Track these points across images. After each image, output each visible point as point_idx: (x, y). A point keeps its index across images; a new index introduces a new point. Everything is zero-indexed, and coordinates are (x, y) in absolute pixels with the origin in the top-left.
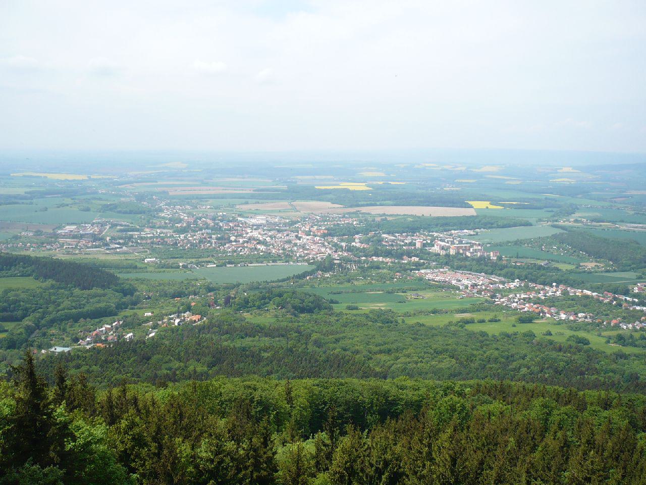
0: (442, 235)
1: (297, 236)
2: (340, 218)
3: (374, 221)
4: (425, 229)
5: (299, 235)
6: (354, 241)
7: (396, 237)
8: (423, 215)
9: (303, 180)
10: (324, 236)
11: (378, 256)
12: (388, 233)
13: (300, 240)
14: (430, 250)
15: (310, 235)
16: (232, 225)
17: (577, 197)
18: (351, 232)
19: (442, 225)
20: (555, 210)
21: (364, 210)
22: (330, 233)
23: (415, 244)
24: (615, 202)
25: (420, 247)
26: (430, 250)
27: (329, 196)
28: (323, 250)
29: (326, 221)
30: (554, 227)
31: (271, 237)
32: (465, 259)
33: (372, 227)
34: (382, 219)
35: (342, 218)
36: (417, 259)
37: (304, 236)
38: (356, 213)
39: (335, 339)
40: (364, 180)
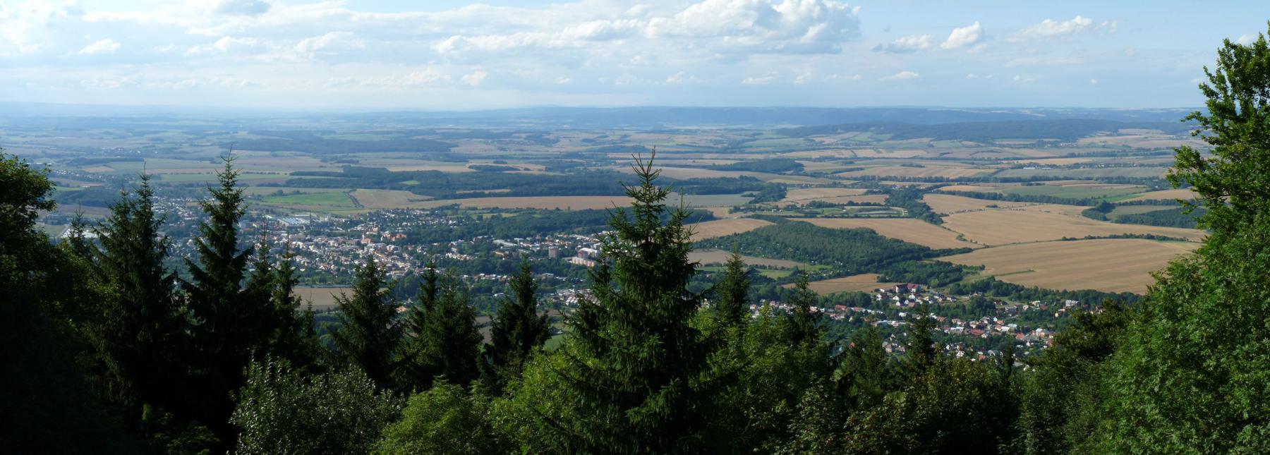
0: (588, 238)
1: (358, 243)
2: (427, 215)
3: (480, 218)
4: (563, 229)
5: (363, 242)
6: (449, 251)
7: (516, 242)
8: (558, 209)
9: (370, 161)
10: (402, 243)
11: (488, 272)
12: (505, 237)
13: (363, 249)
14: (571, 262)
15: (379, 242)
16: (256, 226)
17: (785, 174)
18: (445, 236)
19: (589, 222)
20: (755, 193)
21: (465, 203)
22: (412, 239)
23: (546, 253)
24: (840, 178)
25: (554, 256)
26: (571, 262)
27: (409, 183)
28: (401, 265)
29: (404, 220)
30: (970, 196)
31: (317, 245)
32: (1002, 316)
33: (472, 230)
34: (493, 217)
35: (430, 215)
36: (550, 275)
37: (370, 245)
38: (452, 207)
39: (448, 182)
40: (462, 159)
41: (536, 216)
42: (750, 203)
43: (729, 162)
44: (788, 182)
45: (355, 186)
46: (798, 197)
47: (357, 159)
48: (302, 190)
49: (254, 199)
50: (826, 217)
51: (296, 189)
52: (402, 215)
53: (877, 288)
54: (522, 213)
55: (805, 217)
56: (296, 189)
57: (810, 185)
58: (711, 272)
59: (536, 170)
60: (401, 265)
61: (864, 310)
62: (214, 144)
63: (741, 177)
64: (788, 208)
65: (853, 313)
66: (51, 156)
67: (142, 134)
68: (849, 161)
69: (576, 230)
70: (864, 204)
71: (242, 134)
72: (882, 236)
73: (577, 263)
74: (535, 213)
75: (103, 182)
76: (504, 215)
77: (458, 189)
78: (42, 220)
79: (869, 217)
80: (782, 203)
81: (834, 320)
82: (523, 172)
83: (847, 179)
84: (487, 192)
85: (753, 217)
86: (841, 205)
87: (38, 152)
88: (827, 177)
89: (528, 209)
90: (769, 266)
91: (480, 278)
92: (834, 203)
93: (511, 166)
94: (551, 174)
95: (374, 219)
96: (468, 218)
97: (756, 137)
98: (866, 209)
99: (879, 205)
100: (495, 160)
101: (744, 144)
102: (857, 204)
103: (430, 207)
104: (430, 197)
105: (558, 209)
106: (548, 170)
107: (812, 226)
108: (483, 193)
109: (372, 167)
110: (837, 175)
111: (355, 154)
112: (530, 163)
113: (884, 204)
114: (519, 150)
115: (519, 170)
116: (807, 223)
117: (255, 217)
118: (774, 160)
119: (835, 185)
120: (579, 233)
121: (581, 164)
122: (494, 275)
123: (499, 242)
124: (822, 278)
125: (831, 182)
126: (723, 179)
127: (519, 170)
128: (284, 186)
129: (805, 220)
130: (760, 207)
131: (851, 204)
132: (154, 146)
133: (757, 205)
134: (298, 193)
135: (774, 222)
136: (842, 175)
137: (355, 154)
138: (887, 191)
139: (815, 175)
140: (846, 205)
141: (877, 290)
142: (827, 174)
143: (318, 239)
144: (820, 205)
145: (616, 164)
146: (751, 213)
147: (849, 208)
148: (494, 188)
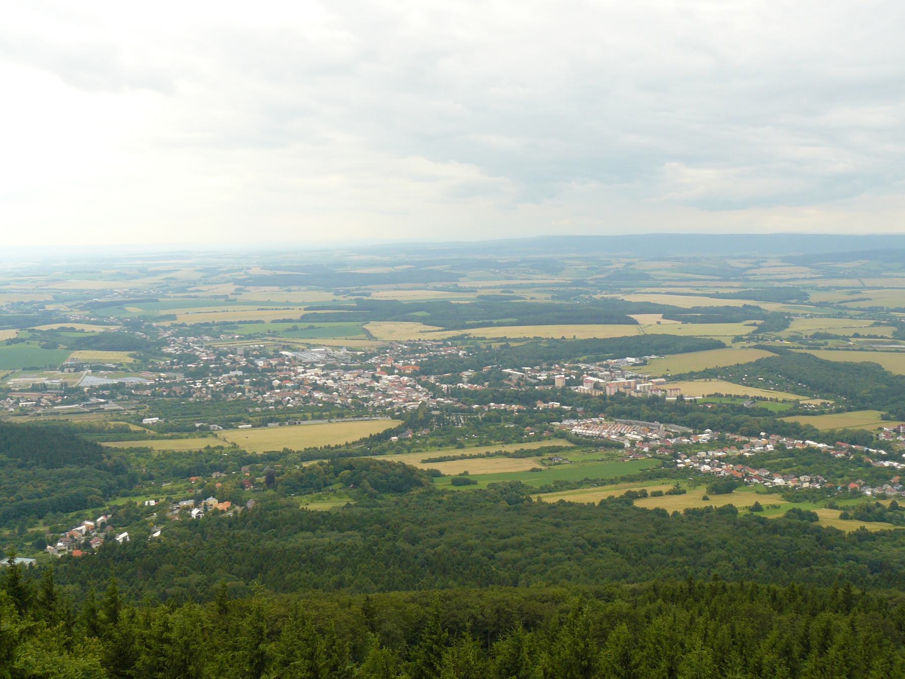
0: (592, 368)
2: (438, 346)
3: (489, 348)
7: (524, 371)
8: (563, 338)
11: (497, 401)
18: (454, 367)
20: (758, 322)
22: (425, 369)
24: (846, 308)
29: (416, 352)
41: (542, 345)
42: (754, 332)
43: (733, 291)
44: (793, 311)
45: (367, 320)
46: (802, 326)
47: (368, 292)
48: (316, 325)
49: (270, 336)
50: (830, 349)
51: (310, 324)
52: (414, 348)
53: (880, 426)
54: (530, 341)
55: (809, 348)
56: (310, 324)
57: (816, 316)
58: (712, 403)
59: (542, 298)
60: (414, 396)
61: (866, 449)
62: (228, 282)
63: (745, 306)
64: (793, 338)
65: (853, 451)
66: (63, 301)
67: (155, 273)
68: (854, 291)
69: (581, 359)
70: (869, 337)
71: (256, 271)
72: (888, 372)
73: (582, 392)
74: (541, 342)
75: (119, 325)
76: (512, 344)
77: (467, 320)
78: (58, 369)
79: (875, 350)
80: (785, 333)
81: (834, 457)
82: (529, 301)
83: (854, 309)
84: (495, 322)
85: (756, 347)
86: (847, 337)
87: (49, 298)
88: (833, 307)
89: (535, 338)
90: (771, 398)
91: (490, 407)
92: (838, 334)
93: (518, 295)
94: (557, 302)
95: (388, 351)
96: (478, 348)
97: (761, 264)
98: (872, 343)
99: (886, 338)
100: (502, 290)
101: (749, 272)
102: (863, 337)
103: (442, 337)
104: (441, 328)
105: (563, 338)
106: (553, 298)
107: (816, 358)
108: (492, 322)
109: (385, 299)
110: (843, 305)
111: (366, 287)
112: (537, 291)
113: (891, 337)
114: (524, 279)
115: (525, 299)
116: (810, 356)
117: (272, 354)
118: (779, 288)
119: (840, 316)
120: (585, 362)
121: (586, 292)
122: (503, 405)
123: (508, 371)
124: (823, 413)
125: (837, 311)
126: (727, 307)
127: (525, 299)
128: (298, 321)
129: (809, 352)
130: (763, 337)
131: (856, 336)
132: (168, 286)
133: (761, 335)
134: (313, 327)
135: (777, 353)
136: (848, 305)
137: (366, 287)
138: (893, 323)
139: (821, 305)
140: (851, 337)
141: (881, 429)
142: (832, 303)
143: (334, 374)
144: (827, 336)
145: (621, 292)
146: (753, 344)
147: (854, 340)
148: (501, 318)
